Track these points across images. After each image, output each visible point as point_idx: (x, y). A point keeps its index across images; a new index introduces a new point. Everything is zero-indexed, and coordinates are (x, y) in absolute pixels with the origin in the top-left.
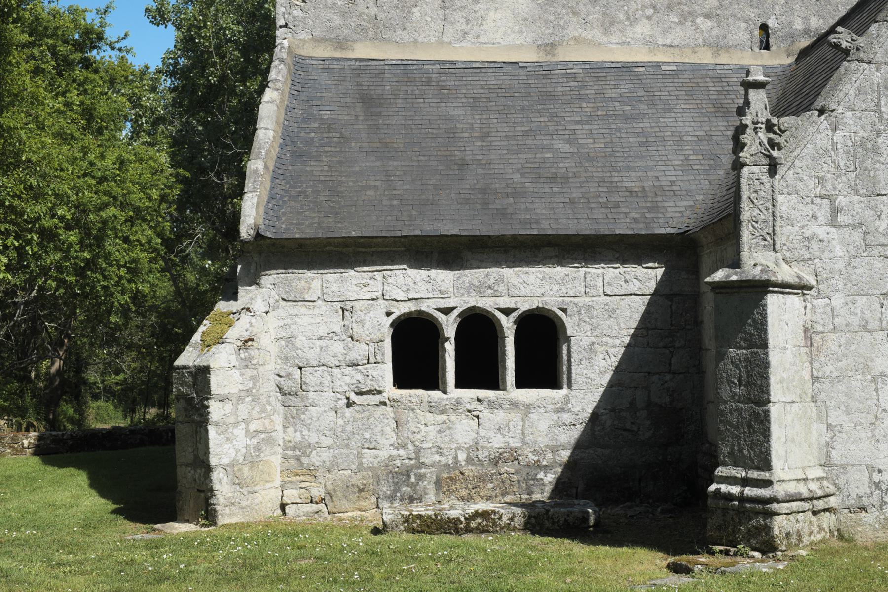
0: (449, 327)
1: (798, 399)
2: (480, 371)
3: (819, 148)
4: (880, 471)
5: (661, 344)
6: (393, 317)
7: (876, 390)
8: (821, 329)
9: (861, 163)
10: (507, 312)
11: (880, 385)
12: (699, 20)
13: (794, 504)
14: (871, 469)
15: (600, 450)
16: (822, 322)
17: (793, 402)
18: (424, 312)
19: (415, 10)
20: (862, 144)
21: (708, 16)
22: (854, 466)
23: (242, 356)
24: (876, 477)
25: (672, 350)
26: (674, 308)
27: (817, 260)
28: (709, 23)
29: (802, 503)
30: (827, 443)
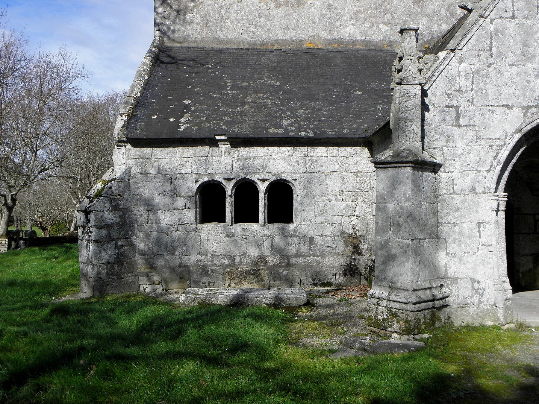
0: (229, 188)
1: (429, 237)
2: (246, 213)
3: (449, 75)
4: (479, 282)
5: (350, 200)
6: (199, 183)
7: (479, 231)
8: (445, 192)
9: (478, 84)
10: (263, 180)
11: (481, 229)
12: (381, 26)
13: (422, 304)
14: (473, 281)
15: (314, 258)
16: (446, 188)
17: (425, 239)
18: (216, 181)
19: (227, 21)
20: (477, 72)
21: (385, 24)
22: (463, 278)
23: (113, 204)
24: (476, 286)
25: (356, 203)
26: (358, 180)
27: (444, 148)
28: (386, 28)
29: (427, 303)
30: (446, 264)
